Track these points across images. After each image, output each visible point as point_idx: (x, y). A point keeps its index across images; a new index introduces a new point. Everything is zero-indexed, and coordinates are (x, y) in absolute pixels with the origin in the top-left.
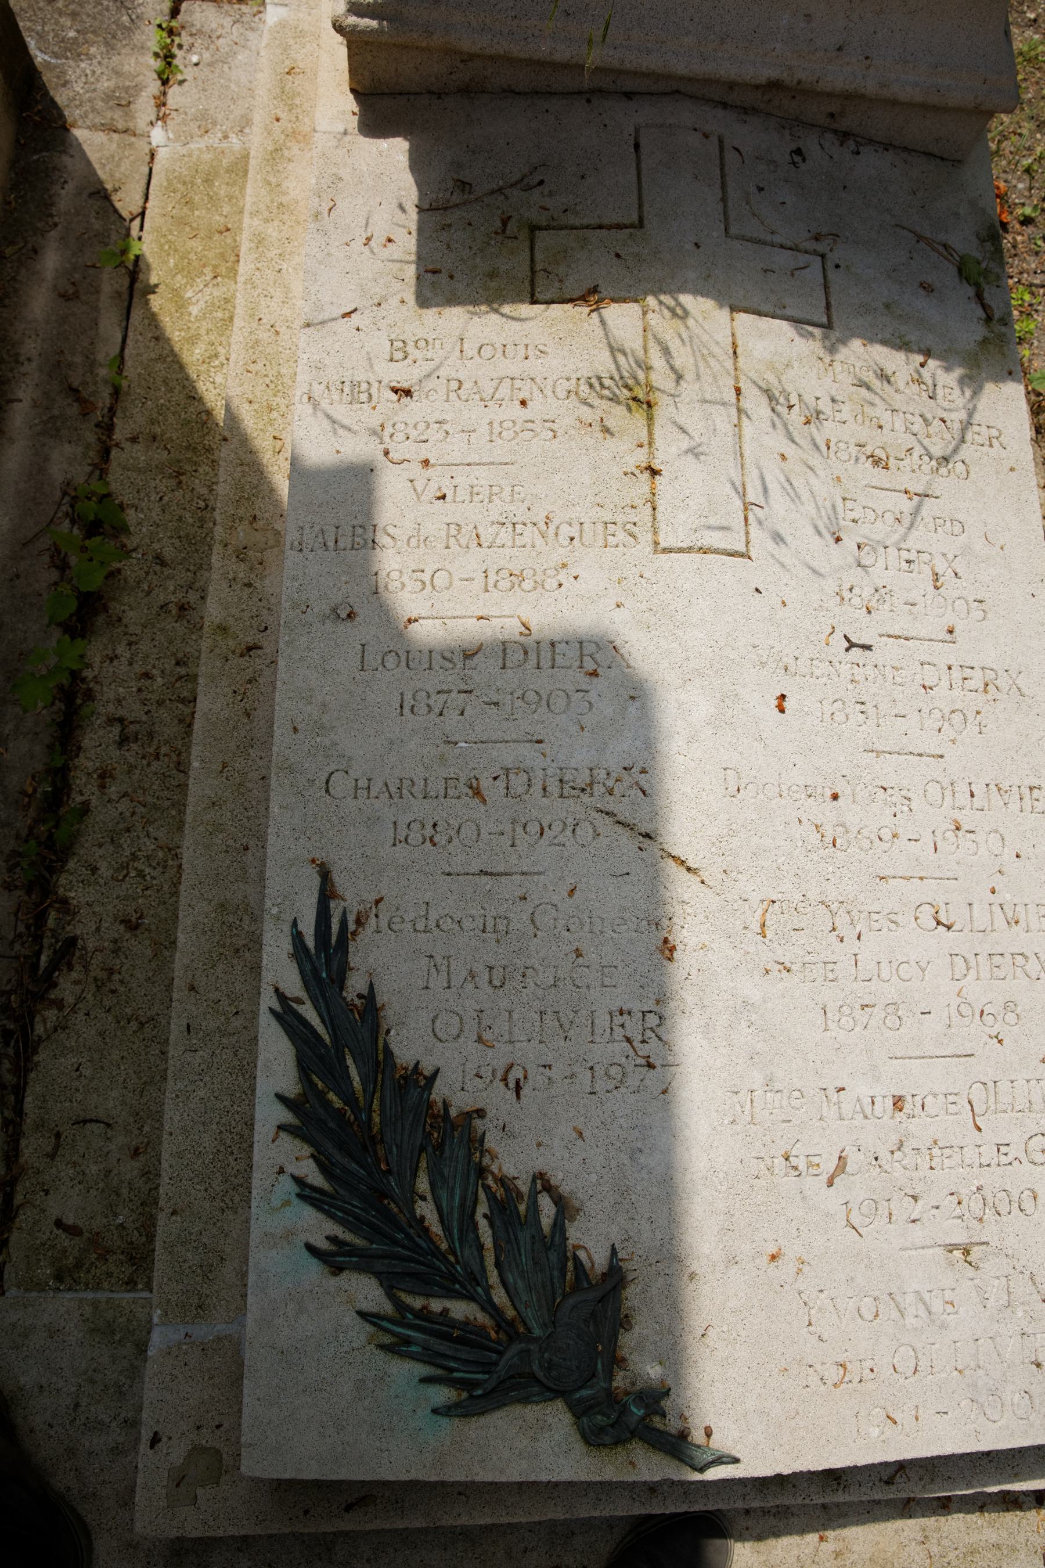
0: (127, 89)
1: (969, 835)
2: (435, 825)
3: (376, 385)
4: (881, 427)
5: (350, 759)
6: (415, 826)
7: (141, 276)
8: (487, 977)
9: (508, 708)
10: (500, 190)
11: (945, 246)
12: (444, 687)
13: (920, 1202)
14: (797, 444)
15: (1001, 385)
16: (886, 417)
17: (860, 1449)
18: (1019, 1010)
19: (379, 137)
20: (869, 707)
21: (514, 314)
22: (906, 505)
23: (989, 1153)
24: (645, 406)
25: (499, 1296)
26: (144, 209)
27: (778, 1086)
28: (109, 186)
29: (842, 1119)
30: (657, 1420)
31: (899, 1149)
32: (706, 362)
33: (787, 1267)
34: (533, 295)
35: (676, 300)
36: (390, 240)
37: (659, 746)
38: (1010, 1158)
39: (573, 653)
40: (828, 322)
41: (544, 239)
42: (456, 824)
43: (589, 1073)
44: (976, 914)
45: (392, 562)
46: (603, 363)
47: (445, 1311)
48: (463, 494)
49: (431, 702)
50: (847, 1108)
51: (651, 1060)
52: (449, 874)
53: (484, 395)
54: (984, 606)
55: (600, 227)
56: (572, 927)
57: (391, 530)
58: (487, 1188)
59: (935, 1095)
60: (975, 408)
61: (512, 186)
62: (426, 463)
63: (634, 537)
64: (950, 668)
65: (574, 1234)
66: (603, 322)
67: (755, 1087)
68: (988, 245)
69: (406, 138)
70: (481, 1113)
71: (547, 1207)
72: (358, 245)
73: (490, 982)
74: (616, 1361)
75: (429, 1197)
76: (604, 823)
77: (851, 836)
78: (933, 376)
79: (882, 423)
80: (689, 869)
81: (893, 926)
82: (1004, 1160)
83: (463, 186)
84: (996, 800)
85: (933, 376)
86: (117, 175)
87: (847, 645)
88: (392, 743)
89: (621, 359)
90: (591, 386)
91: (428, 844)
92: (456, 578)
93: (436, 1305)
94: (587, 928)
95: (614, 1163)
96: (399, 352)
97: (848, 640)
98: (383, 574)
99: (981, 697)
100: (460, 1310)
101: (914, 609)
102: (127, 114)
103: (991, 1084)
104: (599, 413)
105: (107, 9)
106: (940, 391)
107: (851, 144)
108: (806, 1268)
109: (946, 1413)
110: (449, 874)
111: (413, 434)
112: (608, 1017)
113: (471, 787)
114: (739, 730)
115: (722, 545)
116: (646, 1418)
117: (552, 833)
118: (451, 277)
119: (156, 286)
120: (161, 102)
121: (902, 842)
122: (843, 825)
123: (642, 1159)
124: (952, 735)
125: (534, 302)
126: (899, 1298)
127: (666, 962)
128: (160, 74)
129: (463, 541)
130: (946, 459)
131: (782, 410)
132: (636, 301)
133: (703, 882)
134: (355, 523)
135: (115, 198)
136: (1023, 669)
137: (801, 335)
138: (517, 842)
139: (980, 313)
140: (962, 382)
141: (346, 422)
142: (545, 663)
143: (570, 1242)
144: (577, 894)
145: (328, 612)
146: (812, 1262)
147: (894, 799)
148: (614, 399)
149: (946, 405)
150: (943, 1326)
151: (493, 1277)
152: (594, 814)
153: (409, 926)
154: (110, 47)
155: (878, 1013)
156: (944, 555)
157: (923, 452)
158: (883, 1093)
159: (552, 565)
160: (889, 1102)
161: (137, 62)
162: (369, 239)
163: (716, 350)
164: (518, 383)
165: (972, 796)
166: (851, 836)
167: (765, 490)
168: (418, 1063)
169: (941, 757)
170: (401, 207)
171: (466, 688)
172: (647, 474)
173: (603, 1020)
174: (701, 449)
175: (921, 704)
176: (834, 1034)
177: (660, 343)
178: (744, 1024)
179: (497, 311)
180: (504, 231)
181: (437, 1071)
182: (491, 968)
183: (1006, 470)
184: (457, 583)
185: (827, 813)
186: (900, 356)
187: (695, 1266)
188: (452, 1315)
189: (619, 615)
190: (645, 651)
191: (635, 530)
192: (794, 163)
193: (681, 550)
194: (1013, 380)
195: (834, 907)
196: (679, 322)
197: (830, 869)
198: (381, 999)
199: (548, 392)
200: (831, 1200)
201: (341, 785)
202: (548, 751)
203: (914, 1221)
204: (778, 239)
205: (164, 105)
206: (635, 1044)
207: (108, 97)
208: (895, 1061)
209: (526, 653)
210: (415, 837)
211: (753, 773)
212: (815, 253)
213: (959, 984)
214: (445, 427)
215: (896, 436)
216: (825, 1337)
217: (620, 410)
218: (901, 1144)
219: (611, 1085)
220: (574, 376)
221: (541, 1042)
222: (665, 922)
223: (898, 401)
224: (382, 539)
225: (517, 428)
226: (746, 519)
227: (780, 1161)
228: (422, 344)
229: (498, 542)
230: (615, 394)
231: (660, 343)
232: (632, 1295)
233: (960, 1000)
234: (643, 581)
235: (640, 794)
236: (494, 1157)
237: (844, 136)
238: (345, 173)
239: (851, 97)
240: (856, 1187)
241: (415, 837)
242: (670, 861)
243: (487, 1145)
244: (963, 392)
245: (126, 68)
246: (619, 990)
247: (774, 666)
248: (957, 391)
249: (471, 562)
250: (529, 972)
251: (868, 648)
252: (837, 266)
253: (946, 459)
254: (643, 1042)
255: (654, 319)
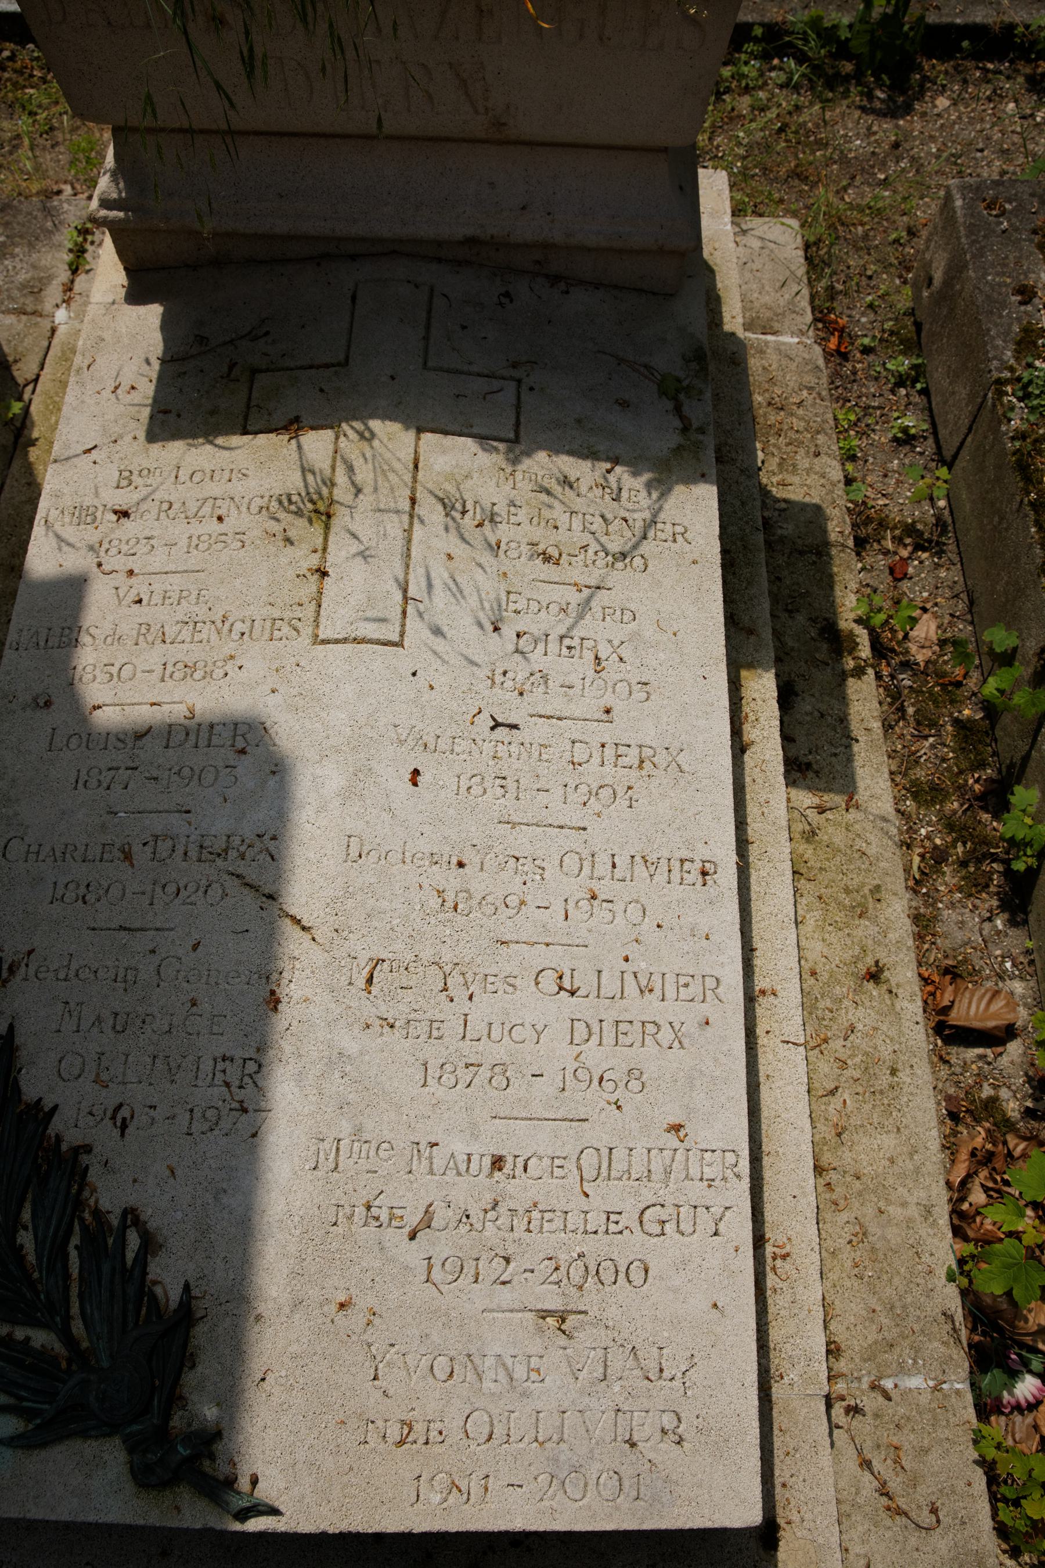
0: (40, 280)
1: (605, 904)
2: (88, 886)
3: (101, 508)
4: (556, 527)
5: (27, 827)
6: (71, 886)
7: (26, 432)
8: (111, 1022)
9: (165, 782)
10: (231, 341)
11: (645, 366)
12: (114, 764)
13: (512, 1265)
14: (468, 543)
15: (692, 487)
16: (563, 519)
17: (417, 1515)
18: (644, 1078)
19: (139, 304)
20: (510, 784)
21: (226, 444)
22: (575, 598)
23: (596, 1220)
24: (324, 518)
25: (78, 1328)
26: (38, 376)
27: (366, 1136)
28: (11, 359)
29: (431, 1172)
30: (207, 1463)
31: (493, 1209)
32: (386, 476)
33: (356, 1319)
34: (245, 427)
35: (366, 425)
36: (133, 388)
37: (291, 815)
38: (620, 1227)
39: (227, 734)
40: (515, 439)
41: (262, 379)
42: (105, 885)
43: (188, 1115)
44: (603, 981)
45: (88, 657)
46: (294, 482)
47: (28, 1339)
48: (157, 599)
49: (102, 778)
50: (439, 1164)
51: (245, 1105)
52: (94, 929)
53: (189, 514)
54: (648, 688)
55: (311, 367)
56: (192, 979)
57: (92, 630)
58: (82, 1220)
59: (541, 1158)
60: (660, 508)
61: (242, 337)
62: (131, 573)
63: (298, 631)
64: (603, 746)
65: (154, 1270)
66: (299, 447)
67: (341, 1136)
68: (694, 365)
69: (161, 304)
70: (88, 1149)
71: (133, 1240)
72: (107, 393)
73: (114, 1028)
74: (174, 1399)
75: (30, 1228)
76: (231, 883)
77: (474, 902)
78: (619, 481)
79: (559, 524)
80: (304, 928)
81: (510, 989)
82: (613, 1228)
83: (201, 340)
84: (640, 869)
85: (619, 481)
86: (20, 349)
87: (493, 723)
88: (63, 813)
89: (310, 478)
90: (280, 502)
91: (80, 902)
92: (139, 670)
93: (20, 1334)
94: (203, 981)
95: (199, 1202)
96: (126, 479)
97: (494, 719)
98: (80, 668)
99: (634, 773)
100: (40, 1338)
101: (571, 692)
102: (37, 299)
103: (605, 1152)
104: (283, 525)
105: (35, 218)
106: (625, 494)
107: (562, 286)
108: (377, 1321)
109: (521, 1486)
110: (94, 929)
111: (124, 548)
112: (211, 1063)
113: (123, 852)
114: (368, 801)
115: (375, 636)
116: (194, 1459)
117: (186, 894)
118: (179, 416)
119: (37, 439)
120: (69, 288)
121: (529, 910)
122: (467, 891)
123: (225, 1200)
124: (597, 807)
125: (245, 432)
126: (477, 1360)
127: (270, 1013)
128: (70, 265)
129: (150, 639)
130: (624, 555)
131: (457, 515)
132: (332, 428)
133: (314, 939)
134: (64, 625)
135: (14, 368)
136: (685, 746)
137: (484, 450)
138: (155, 901)
139: (677, 423)
140: (649, 486)
141: (71, 540)
142: (202, 743)
143: (150, 1277)
144: (200, 948)
145: (30, 701)
146: (384, 1314)
147: (526, 868)
148: (299, 513)
149: (630, 506)
150: (525, 1394)
151: (75, 1309)
152: (226, 877)
153: (51, 975)
154: (31, 245)
155: (484, 1073)
156: (610, 641)
157: (599, 548)
158: (481, 1151)
159: (222, 657)
160: (487, 1162)
161: (53, 257)
162: (116, 388)
163: (397, 466)
164: (219, 502)
165: (614, 866)
166: (474, 902)
167: (430, 586)
168: (40, 1099)
169: (584, 829)
170: (148, 362)
171: (132, 765)
172: (316, 576)
173: (207, 1065)
174: (368, 553)
175: (567, 780)
176: (432, 1090)
177: (345, 461)
178: (337, 1075)
179: (211, 443)
180: (229, 375)
181: (56, 1107)
182: (116, 1014)
183: (688, 562)
184: (139, 675)
185: (451, 881)
186: (586, 465)
187: (262, 1308)
188: (33, 1344)
189: (272, 700)
190: (290, 732)
191: (299, 624)
192: (501, 304)
193: (337, 641)
194: (706, 482)
195: (447, 969)
196: (366, 443)
197: (448, 932)
198: (18, 1041)
199: (244, 509)
200: (413, 1254)
201: (16, 849)
202: (193, 820)
203: (504, 1283)
204: (474, 368)
205: (71, 290)
206: (234, 1089)
207: (23, 286)
208: (497, 1121)
209: (187, 734)
210: (70, 896)
211: (378, 840)
212: (512, 378)
213: (578, 1049)
214: (152, 542)
215: (571, 534)
216: (391, 1392)
217: (302, 522)
218: (496, 1204)
219: (206, 1127)
220: (267, 494)
221: (151, 1084)
222: (275, 976)
223: (579, 504)
224: (85, 639)
225: (212, 541)
226: (404, 613)
227: (360, 1211)
228: (145, 472)
229: (180, 638)
230: (299, 508)
231: (345, 461)
232: (200, 1332)
233: (577, 1065)
234: (299, 669)
235: (269, 859)
236: (94, 1190)
237: (555, 279)
238: (107, 335)
239: (546, 246)
240: (440, 1244)
241: (70, 896)
242: (288, 921)
243: (89, 1179)
244: (650, 494)
245: (43, 262)
246: (225, 1038)
247: (413, 744)
248: (644, 493)
249: (153, 657)
250: (148, 1019)
251: (515, 727)
252: (531, 389)
253: (624, 555)
254: (241, 1087)
255: (343, 442)
